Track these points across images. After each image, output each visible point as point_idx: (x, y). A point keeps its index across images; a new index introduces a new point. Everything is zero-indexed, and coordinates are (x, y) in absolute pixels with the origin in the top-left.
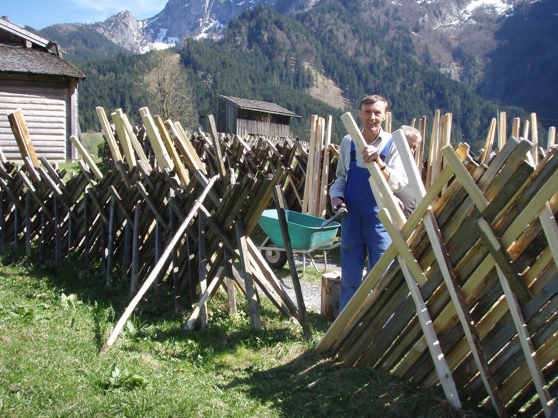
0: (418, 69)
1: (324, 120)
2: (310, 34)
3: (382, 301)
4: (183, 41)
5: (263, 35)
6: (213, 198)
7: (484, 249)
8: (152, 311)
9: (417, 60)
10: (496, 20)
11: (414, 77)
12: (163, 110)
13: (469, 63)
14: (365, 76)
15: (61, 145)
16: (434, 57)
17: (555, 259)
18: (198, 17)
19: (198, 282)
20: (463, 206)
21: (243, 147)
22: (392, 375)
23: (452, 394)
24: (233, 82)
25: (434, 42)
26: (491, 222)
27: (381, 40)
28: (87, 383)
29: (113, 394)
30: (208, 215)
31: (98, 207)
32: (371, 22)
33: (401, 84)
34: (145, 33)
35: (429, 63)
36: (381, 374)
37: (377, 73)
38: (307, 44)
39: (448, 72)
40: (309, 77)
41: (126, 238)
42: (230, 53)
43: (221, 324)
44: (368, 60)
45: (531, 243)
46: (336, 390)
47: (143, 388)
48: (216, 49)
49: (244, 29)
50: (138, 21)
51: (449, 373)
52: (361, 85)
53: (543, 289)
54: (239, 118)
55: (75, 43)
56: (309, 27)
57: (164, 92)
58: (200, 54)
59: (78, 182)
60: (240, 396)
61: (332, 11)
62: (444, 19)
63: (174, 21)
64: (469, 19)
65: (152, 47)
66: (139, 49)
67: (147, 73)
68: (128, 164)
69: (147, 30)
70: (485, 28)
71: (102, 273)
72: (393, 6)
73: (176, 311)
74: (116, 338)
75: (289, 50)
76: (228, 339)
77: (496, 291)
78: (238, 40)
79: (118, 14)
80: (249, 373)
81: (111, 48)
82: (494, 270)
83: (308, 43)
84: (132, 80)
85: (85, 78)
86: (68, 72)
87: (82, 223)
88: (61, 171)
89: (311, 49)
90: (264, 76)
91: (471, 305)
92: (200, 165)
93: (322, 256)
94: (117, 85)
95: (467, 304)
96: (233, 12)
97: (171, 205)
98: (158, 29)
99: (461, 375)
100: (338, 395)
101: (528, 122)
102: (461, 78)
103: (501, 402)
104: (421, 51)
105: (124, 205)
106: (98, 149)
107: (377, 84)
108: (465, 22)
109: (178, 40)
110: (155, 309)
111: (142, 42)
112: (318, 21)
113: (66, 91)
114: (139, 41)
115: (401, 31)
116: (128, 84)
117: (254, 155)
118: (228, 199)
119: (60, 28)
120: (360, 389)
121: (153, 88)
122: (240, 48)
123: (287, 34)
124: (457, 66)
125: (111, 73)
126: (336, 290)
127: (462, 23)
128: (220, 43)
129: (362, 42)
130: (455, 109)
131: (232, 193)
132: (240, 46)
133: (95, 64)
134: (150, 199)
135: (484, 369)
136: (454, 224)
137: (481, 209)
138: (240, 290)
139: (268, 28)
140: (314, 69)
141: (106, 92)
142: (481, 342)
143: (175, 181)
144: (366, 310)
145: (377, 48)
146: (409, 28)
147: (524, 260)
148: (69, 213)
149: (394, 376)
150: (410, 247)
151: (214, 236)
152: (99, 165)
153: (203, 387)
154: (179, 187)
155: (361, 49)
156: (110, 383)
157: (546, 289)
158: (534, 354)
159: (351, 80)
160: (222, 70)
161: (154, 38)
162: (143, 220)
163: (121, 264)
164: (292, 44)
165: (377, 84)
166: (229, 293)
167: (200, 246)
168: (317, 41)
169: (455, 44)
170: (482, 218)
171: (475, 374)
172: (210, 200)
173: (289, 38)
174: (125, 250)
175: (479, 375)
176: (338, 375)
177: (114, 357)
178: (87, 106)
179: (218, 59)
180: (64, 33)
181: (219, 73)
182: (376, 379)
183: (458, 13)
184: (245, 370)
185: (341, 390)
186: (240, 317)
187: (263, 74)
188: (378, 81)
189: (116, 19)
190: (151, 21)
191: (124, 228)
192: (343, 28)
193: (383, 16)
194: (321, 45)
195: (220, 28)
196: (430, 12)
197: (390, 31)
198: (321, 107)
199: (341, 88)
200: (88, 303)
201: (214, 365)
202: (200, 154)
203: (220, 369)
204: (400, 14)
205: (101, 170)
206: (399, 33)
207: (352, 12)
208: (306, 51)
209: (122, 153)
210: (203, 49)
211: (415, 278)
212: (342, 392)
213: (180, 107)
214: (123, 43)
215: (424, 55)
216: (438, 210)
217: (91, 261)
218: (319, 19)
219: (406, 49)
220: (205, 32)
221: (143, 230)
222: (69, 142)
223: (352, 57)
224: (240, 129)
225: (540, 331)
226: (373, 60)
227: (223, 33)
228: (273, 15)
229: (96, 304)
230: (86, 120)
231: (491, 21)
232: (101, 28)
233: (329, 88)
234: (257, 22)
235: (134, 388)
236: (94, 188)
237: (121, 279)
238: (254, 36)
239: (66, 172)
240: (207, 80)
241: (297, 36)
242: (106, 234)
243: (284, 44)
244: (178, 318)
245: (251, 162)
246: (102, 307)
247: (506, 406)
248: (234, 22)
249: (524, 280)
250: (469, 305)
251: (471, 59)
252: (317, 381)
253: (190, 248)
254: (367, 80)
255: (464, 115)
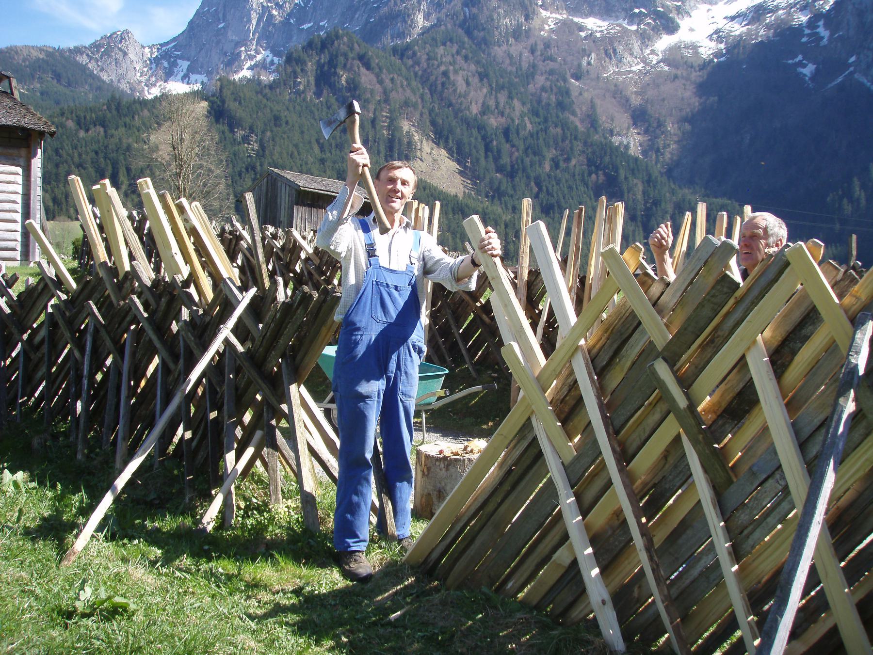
0: (579, 136)
1: (427, 208)
2: (413, 77)
3: (507, 487)
4: (214, 82)
5: (340, 77)
6: (249, 323)
7: (662, 407)
8: (148, 499)
9: (578, 123)
10: (699, 65)
11: (572, 149)
12: (179, 188)
13: (657, 131)
14: (497, 146)
15: (13, 238)
16: (604, 118)
17: (770, 424)
18: (238, 44)
19: (221, 456)
20: (632, 340)
21: (301, 248)
22: (520, 602)
23: (611, 630)
24: (291, 148)
25: (604, 96)
26: (675, 365)
27: (522, 90)
28: (38, 609)
29: (79, 626)
30: (240, 348)
31: (67, 335)
32: (508, 61)
33: (553, 160)
34: (154, 66)
35: (596, 129)
36: (503, 599)
37: (516, 142)
38: (408, 93)
39: (625, 143)
40: (410, 144)
41: (111, 385)
42: (287, 103)
43: (257, 521)
44: (503, 120)
45: (734, 398)
46: (433, 624)
47: (128, 619)
48: (265, 96)
49: (310, 66)
50: (144, 47)
51: (606, 596)
52: (491, 159)
53: (750, 469)
54: (297, 204)
55: (40, 78)
56: (413, 66)
57: (181, 160)
58: (240, 103)
59: (36, 294)
60: (282, 632)
61: (448, 43)
62: (620, 61)
63: (201, 49)
64: (658, 62)
65: (164, 89)
66: (143, 91)
67: (155, 129)
68: (116, 268)
69: (157, 61)
70: (683, 77)
71: (71, 439)
72: (543, 39)
73: (187, 500)
74: (88, 539)
75: (379, 101)
76: (267, 545)
77: (681, 472)
78: (300, 82)
79: (112, 35)
80: (298, 597)
81: (99, 88)
82: (677, 439)
83: (409, 91)
84: (130, 140)
85: (54, 132)
86: (27, 122)
87: (41, 360)
88: (9, 276)
89: (414, 100)
90: (339, 141)
91: (642, 493)
92: (230, 272)
93: (419, 420)
94: (106, 147)
95: (636, 492)
96: (294, 38)
97: (183, 333)
98: (176, 61)
99: (624, 599)
100: (436, 631)
101: (739, 219)
102: (645, 153)
103: (685, 642)
104: (584, 109)
105: (108, 333)
106: (72, 247)
107: (514, 158)
108: (652, 67)
109: (205, 80)
110: (152, 496)
111: (148, 80)
112: (425, 57)
113: (23, 152)
114: (143, 79)
115: (554, 77)
116: (125, 145)
117: (317, 261)
118: (272, 325)
119: (17, 53)
120: (470, 622)
121: (164, 153)
122: (303, 96)
123: (377, 76)
124: (639, 134)
125: (98, 127)
126: (438, 470)
127: (648, 68)
128: (272, 86)
129: (494, 93)
130: (634, 200)
131: (278, 315)
132: (303, 92)
133: (72, 113)
134: (150, 324)
135: (661, 591)
136: (618, 368)
137: (660, 345)
138: (289, 470)
139: (348, 66)
140: (417, 132)
141: (88, 158)
142: (655, 550)
143: (190, 296)
144: (481, 500)
145: (516, 103)
146: (566, 73)
147: (724, 425)
148: (20, 344)
149: (524, 603)
150: (551, 403)
151: (249, 383)
152: (72, 272)
153: (221, 617)
154: (196, 305)
155: (492, 103)
156: (76, 610)
157: (755, 469)
158: (736, 568)
159: (474, 151)
160: (275, 129)
161: (169, 75)
162: (138, 356)
163: (101, 426)
164: (385, 92)
165: (514, 158)
166: (271, 471)
167: (226, 399)
168: (423, 88)
169: (636, 101)
170: (660, 359)
171: (647, 600)
172: (245, 326)
173: (381, 82)
174: (109, 402)
175: (653, 601)
176: (436, 601)
177: (85, 570)
178: (57, 178)
179: (269, 111)
180: (24, 60)
181: (268, 134)
182: (495, 607)
183: (642, 53)
184: (292, 592)
185: (441, 624)
186: (286, 510)
187: (338, 138)
188: (516, 154)
189: (109, 43)
190: (164, 48)
191: (109, 368)
192: (464, 70)
193: (526, 54)
194: (429, 96)
195: (272, 63)
196: (599, 50)
197: (537, 77)
198: (427, 191)
199: (459, 162)
200: (46, 486)
201: (243, 583)
202: (232, 258)
203: (252, 591)
204: (553, 51)
205: (75, 279)
206: (551, 81)
207: (478, 45)
208: (406, 103)
209: (110, 254)
210: (245, 95)
211: (557, 449)
212: (442, 627)
213: (205, 185)
214: (119, 81)
215: (589, 116)
216: (594, 346)
217: (54, 421)
218: (428, 54)
219: (561, 106)
220: (248, 69)
221: (138, 372)
222: (27, 233)
223: (476, 115)
224: (299, 221)
225: (746, 532)
226: (509, 120)
227: (277, 71)
228: (356, 45)
229: (59, 486)
230: (55, 200)
231: (692, 67)
232: (84, 56)
233: (439, 161)
234: (331, 55)
235: (114, 618)
236: (62, 304)
237: (101, 449)
238: (325, 78)
239: (17, 279)
240: (249, 144)
241: (392, 80)
242: (79, 378)
243: (372, 92)
244: (190, 510)
245: (313, 272)
246: (69, 493)
247: (693, 649)
248: (294, 55)
249: (722, 456)
250: (640, 492)
251: (660, 125)
252: (403, 610)
253: (210, 401)
254: (499, 151)
255: (647, 210)
